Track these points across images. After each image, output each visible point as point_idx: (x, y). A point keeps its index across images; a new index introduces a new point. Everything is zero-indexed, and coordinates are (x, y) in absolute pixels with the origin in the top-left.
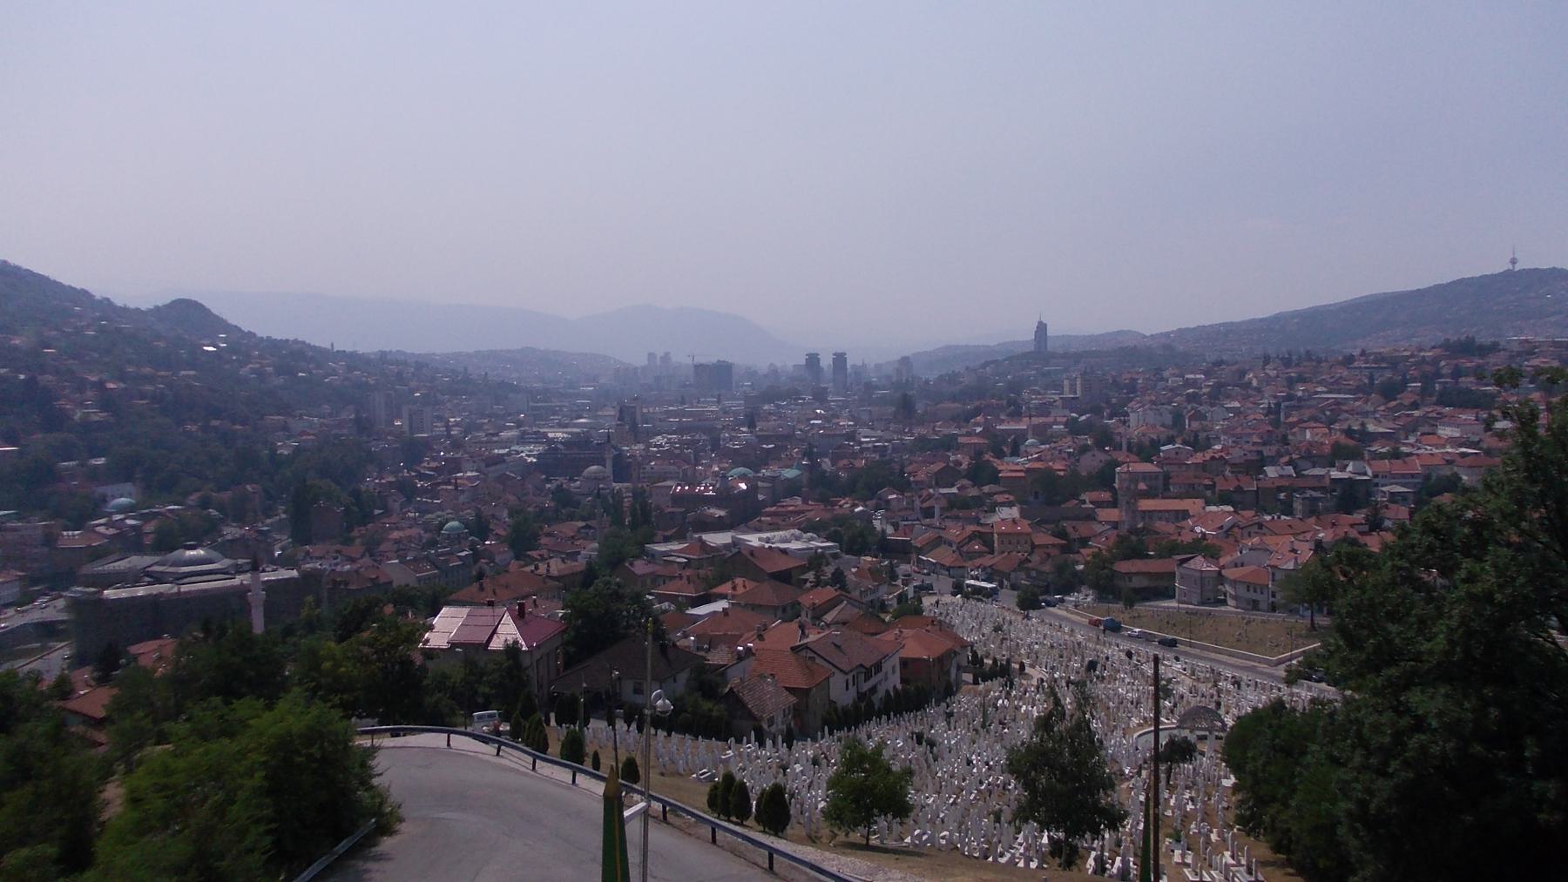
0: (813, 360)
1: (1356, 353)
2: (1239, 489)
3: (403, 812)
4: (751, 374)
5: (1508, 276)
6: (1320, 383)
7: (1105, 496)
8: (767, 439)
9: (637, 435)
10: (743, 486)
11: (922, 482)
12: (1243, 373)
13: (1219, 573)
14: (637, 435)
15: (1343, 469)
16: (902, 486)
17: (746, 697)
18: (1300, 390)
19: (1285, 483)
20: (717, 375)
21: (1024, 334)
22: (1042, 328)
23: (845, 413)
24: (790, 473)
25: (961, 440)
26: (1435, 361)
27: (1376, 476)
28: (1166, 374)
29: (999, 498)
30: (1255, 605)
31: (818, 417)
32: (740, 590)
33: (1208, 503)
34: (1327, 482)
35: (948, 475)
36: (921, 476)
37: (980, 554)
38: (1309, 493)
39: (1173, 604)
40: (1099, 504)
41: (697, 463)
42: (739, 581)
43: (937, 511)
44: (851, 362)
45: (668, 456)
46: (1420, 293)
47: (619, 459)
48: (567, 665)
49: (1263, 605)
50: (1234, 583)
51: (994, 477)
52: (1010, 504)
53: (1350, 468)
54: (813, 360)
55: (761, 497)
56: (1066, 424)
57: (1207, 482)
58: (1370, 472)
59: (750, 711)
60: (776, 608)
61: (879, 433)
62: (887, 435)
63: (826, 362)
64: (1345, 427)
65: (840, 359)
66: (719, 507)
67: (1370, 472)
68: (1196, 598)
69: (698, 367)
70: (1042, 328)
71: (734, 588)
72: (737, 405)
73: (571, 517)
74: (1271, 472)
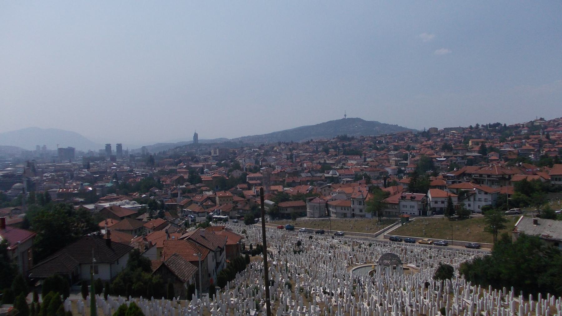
0: (108, 146)
1: (310, 140)
2: (294, 182)
3: (41, 145)
4: (81, 153)
5: (344, 119)
6: (301, 150)
7: (245, 186)
8: (95, 173)
9: (35, 173)
10: (91, 189)
11: (169, 184)
12: (273, 148)
13: (326, 203)
14: (35, 173)
15: (328, 173)
16: (160, 187)
17: (172, 268)
18: (295, 152)
19: (308, 179)
20: (69, 152)
21: (189, 138)
22: (196, 136)
23: (125, 165)
24: (109, 185)
25: (178, 170)
26: (336, 143)
27: (340, 175)
28: (245, 149)
29: (204, 188)
30: (345, 215)
31: (114, 166)
32: (110, 224)
33: (284, 187)
34: (323, 178)
35: (181, 181)
36: (168, 182)
37: (212, 206)
38: (319, 182)
39: (307, 218)
40: (243, 189)
41: (66, 182)
42: (109, 220)
43: (179, 194)
44: (124, 148)
45: (52, 180)
46: (317, 126)
47: (29, 182)
48: (35, 261)
49: (349, 215)
50: (335, 207)
51: (200, 181)
52: (209, 191)
53: (331, 173)
54: (108, 146)
55: (98, 194)
56: (217, 165)
57: (281, 180)
58: (338, 174)
59: (177, 277)
60: (132, 230)
61: (143, 170)
62: (146, 170)
63: (114, 149)
64: (318, 162)
65: (119, 146)
66: (80, 197)
67: (338, 174)
68: (317, 215)
69: (60, 149)
70: (196, 136)
71: (107, 224)
72: (80, 163)
73: (8, 206)
74: (303, 175)
